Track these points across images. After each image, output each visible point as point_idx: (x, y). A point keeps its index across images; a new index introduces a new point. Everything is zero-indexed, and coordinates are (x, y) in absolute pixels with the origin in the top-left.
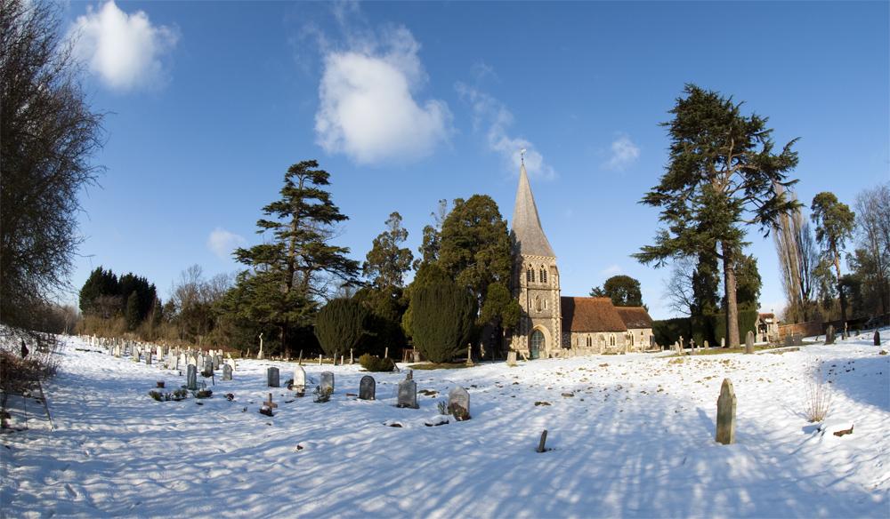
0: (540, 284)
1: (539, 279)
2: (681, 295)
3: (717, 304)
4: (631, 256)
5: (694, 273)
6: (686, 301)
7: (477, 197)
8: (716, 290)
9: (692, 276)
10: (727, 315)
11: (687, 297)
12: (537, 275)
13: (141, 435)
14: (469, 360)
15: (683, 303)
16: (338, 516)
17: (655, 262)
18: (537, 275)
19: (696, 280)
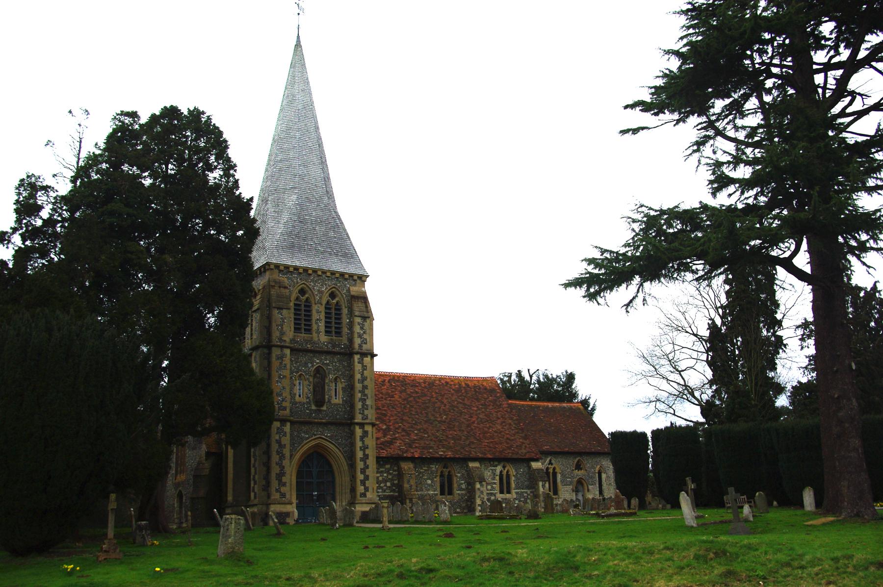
0: (324, 338)
1: (322, 325)
2: (676, 377)
3: (202, 145)
4: (567, 285)
5: (713, 327)
6: (687, 392)
7: (171, 112)
8: (773, 368)
9: (706, 334)
10: (490, 460)
11: (691, 384)
12: (318, 314)
13: (412, 459)
14: (649, 435)
15: (680, 396)
16: (199, 584)
17: (623, 293)
18: (318, 314)
19: (716, 341)
